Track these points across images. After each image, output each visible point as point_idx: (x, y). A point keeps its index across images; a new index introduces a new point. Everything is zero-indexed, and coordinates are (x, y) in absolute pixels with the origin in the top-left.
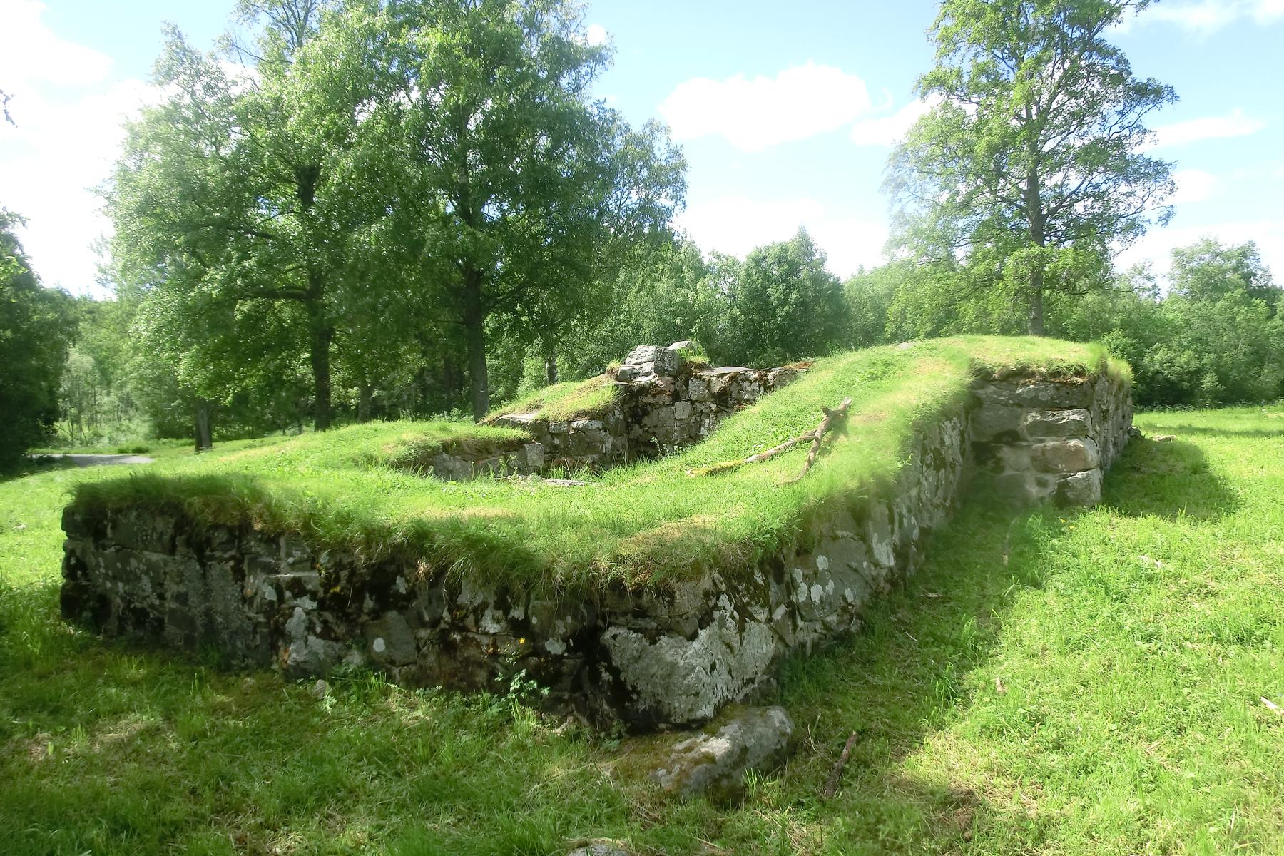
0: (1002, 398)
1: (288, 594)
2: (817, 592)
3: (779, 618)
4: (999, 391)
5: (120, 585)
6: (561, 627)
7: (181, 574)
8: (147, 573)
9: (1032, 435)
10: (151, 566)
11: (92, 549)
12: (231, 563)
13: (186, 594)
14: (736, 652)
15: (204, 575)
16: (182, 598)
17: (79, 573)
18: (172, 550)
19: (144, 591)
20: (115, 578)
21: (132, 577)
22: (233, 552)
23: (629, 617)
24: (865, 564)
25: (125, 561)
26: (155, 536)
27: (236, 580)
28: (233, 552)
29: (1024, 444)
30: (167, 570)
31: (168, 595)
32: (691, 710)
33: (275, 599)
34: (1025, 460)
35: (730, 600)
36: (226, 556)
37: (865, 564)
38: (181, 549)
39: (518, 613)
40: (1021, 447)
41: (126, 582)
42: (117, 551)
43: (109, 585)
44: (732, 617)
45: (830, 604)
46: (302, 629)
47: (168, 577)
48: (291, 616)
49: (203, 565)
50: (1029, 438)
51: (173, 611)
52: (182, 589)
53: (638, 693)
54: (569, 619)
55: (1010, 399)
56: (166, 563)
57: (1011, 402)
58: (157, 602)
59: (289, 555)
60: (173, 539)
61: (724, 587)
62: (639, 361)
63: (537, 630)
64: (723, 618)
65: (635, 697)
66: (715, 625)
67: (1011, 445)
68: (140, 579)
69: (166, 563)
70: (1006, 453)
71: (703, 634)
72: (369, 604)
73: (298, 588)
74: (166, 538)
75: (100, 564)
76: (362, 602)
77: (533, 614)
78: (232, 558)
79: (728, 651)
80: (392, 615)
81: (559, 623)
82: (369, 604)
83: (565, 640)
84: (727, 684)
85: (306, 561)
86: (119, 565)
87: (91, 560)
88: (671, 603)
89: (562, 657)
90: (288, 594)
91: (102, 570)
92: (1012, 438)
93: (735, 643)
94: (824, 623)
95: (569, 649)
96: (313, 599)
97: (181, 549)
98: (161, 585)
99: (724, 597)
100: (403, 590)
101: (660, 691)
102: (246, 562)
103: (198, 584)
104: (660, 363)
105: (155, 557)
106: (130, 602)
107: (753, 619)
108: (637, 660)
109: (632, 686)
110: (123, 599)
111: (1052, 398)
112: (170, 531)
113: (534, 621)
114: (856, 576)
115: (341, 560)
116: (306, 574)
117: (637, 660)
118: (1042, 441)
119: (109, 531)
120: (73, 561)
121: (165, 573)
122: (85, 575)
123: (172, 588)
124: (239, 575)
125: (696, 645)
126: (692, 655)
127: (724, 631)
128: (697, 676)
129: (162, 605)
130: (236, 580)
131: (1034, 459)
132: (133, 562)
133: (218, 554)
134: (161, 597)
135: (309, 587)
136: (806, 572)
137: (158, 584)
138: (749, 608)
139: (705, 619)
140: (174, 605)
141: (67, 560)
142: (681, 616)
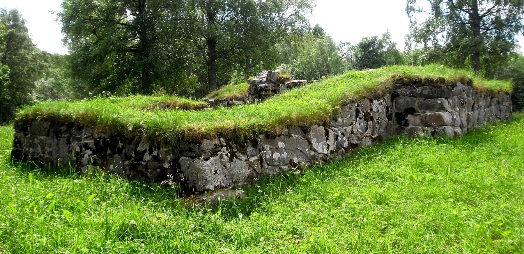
0: (408, 93)
1: (83, 149)
2: (276, 156)
3: (252, 161)
4: (406, 90)
5: (31, 149)
6: (169, 158)
7: (51, 144)
8: (39, 144)
9: (421, 109)
10: (41, 141)
11: (23, 136)
12: (67, 138)
13: (52, 151)
14: (227, 169)
15: (58, 144)
16: (50, 153)
17: (18, 145)
18: (48, 135)
19: (38, 151)
20: (29, 146)
21: (35, 146)
22: (68, 135)
23: (187, 152)
24: (307, 150)
25: (33, 140)
26: (43, 129)
27: (67, 144)
28: (68, 135)
29: (418, 113)
30: (47, 142)
31: (46, 152)
32: (204, 186)
33: (79, 151)
34: (418, 121)
35: (227, 149)
36: (65, 136)
37: (307, 150)
38: (51, 134)
39: (155, 153)
40: (416, 115)
41: (33, 148)
42: (31, 136)
43: (27, 149)
44: (227, 155)
45: (284, 161)
46: (87, 162)
47: (46, 145)
48: (83, 157)
49: (58, 140)
50: (420, 111)
51: (47, 158)
52: (51, 149)
53: (189, 180)
54: (171, 155)
55: (411, 93)
56: (46, 139)
57: (412, 95)
58: (42, 155)
59: (85, 134)
60: (49, 130)
61: (225, 144)
62: (262, 77)
63: (161, 159)
64: (222, 155)
65: (188, 182)
66: (218, 157)
67: (412, 114)
68: (37, 146)
69: (46, 139)
70: (409, 117)
71: (211, 159)
72: (109, 151)
73: (87, 146)
74: (47, 130)
75: (25, 142)
76: (107, 151)
77: (160, 153)
78: (67, 136)
79: (224, 168)
80: (116, 156)
81: (168, 157)
82: (109, 151)
83: (170, 163)
84: (223, 180)
85: (90, 136)
86: (31, 141)
87: (22, 140)
88: (199, 146)
89: (168, 169)
90: (83, 149)
91: (26, 144)
92: (412, 111)
93: (228, 165)
94: (280, 169)
95: (170, 166)
96: (91, 150)
97: (51, 134)
98: (44, 148)
99: (225, 148)
100: (120, 147)
101: (195, 179)
102: (72, 138)
103: (56, 147)
104: (269, 78)
105: (43, 138)
106: (33, 155)
107: (237, 158)
108: (188, 168)
109: (187, 178)
110: (31, 154)
111: (429, 93)
112: (48, 127)
113: (161, 156)
114: (301, 153)
115: (101, 136)
116: (90, 141)
117: (188, 168)
118: (425, 112)
119: (29, 128)
120: (16, 141)
121: (46, 144)
122: (20, 145)
123: (48, 149)
124: (69, 142)
125: (208, 162)
126: (206, 166)
127: (222, 160)
128: (206, 173)
129: (44, 156)
130: (67, 144)
131: (422, 120)
132: (36, 140)
133: (63, 135)
134: (44, 153)
135: (91, 146)
136: (272, 147)
137: (43, 148)
138: (236, 154)
139: (214, 153)
140: (48, 156)
141: (15, 140)
142: (203, 151)
